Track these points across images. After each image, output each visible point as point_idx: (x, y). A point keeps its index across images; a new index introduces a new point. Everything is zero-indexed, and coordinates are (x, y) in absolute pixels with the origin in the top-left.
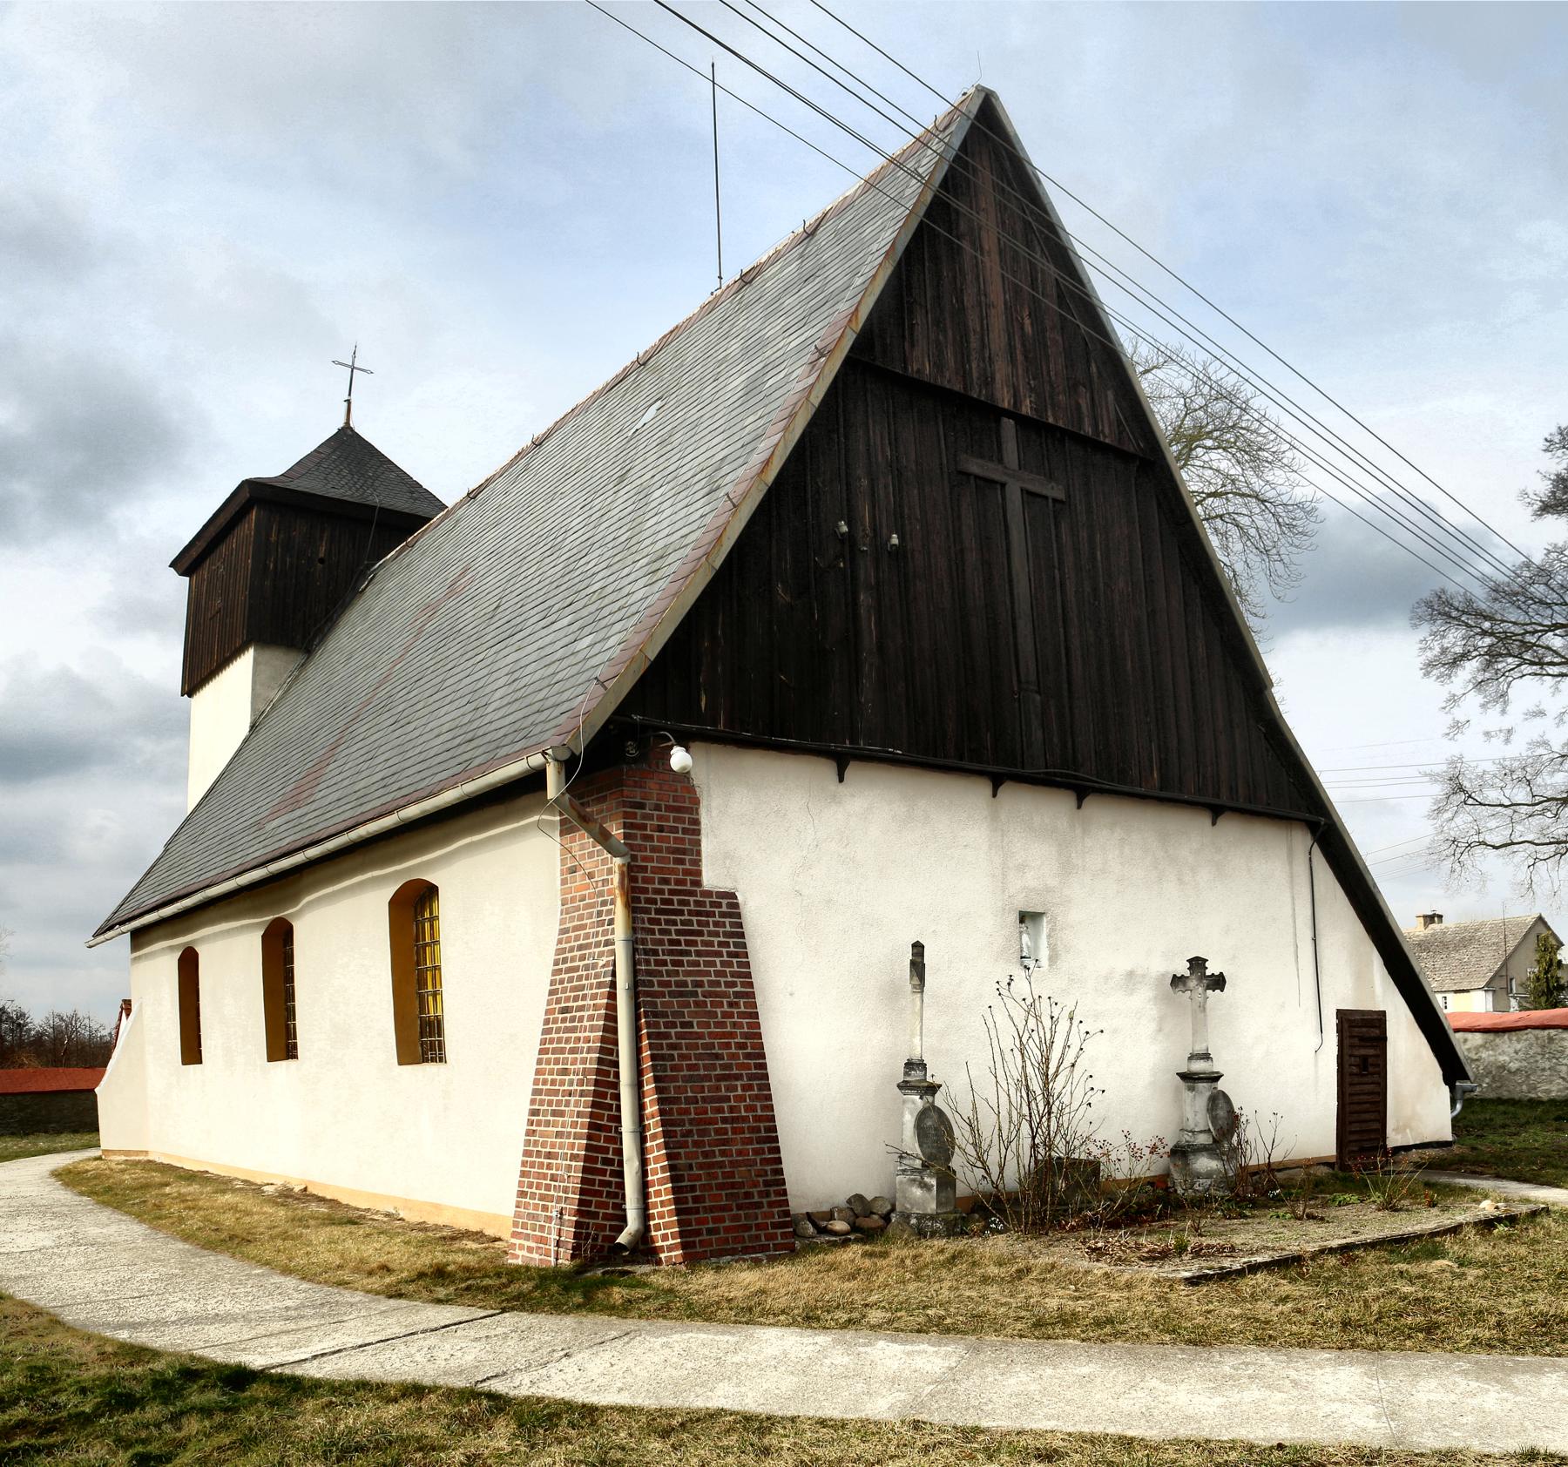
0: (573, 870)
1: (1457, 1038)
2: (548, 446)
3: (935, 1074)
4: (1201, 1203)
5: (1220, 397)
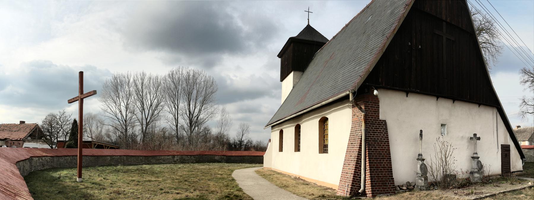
0: (354, 115)
1: (523, 150)
2: (349, 26)
3: (424, 157)
4: (476, 183)
5: (487, 22)
